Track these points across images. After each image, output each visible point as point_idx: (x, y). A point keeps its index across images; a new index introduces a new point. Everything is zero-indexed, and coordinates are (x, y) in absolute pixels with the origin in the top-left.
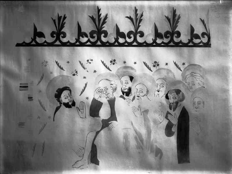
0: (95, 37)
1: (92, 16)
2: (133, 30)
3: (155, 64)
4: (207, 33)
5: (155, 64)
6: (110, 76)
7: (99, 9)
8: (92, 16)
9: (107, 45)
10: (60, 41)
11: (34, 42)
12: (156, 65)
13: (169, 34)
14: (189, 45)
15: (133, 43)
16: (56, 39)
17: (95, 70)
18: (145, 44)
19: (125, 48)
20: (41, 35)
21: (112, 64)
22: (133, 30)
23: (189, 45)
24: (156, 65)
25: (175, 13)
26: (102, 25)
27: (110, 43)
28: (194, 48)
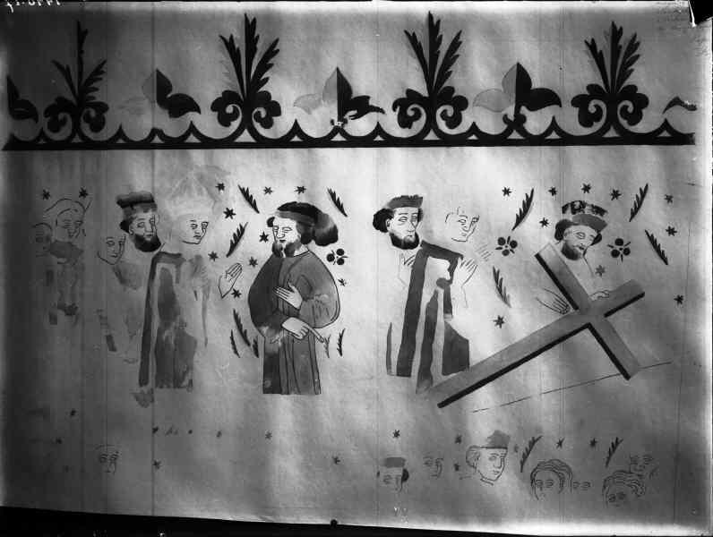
0: (412, 109)
1: (618, 28)
2: (421, 88)
3: (618, 248)
4: (602, 85)
5: (618, 248)
6: (203, 286)
7: (228, 38)
8: (618, 28)
9: (473, 140)
10: (254, 133)
11: (77, 136)
12: (621, 252)
13: (61, 111)
14: (607, 135)
15: (426, 136)
16: (240, 125)
17: (676, 297)
18: (473, 137)
19: (468, 149)
20: (362, 106)
21: (624, 256)
22: (421, 88)
23: (607, 135)
24: (621, 252)
25: (234, 47)
26: (626, 53)
27: (169, 137)
28: (128, 152)
